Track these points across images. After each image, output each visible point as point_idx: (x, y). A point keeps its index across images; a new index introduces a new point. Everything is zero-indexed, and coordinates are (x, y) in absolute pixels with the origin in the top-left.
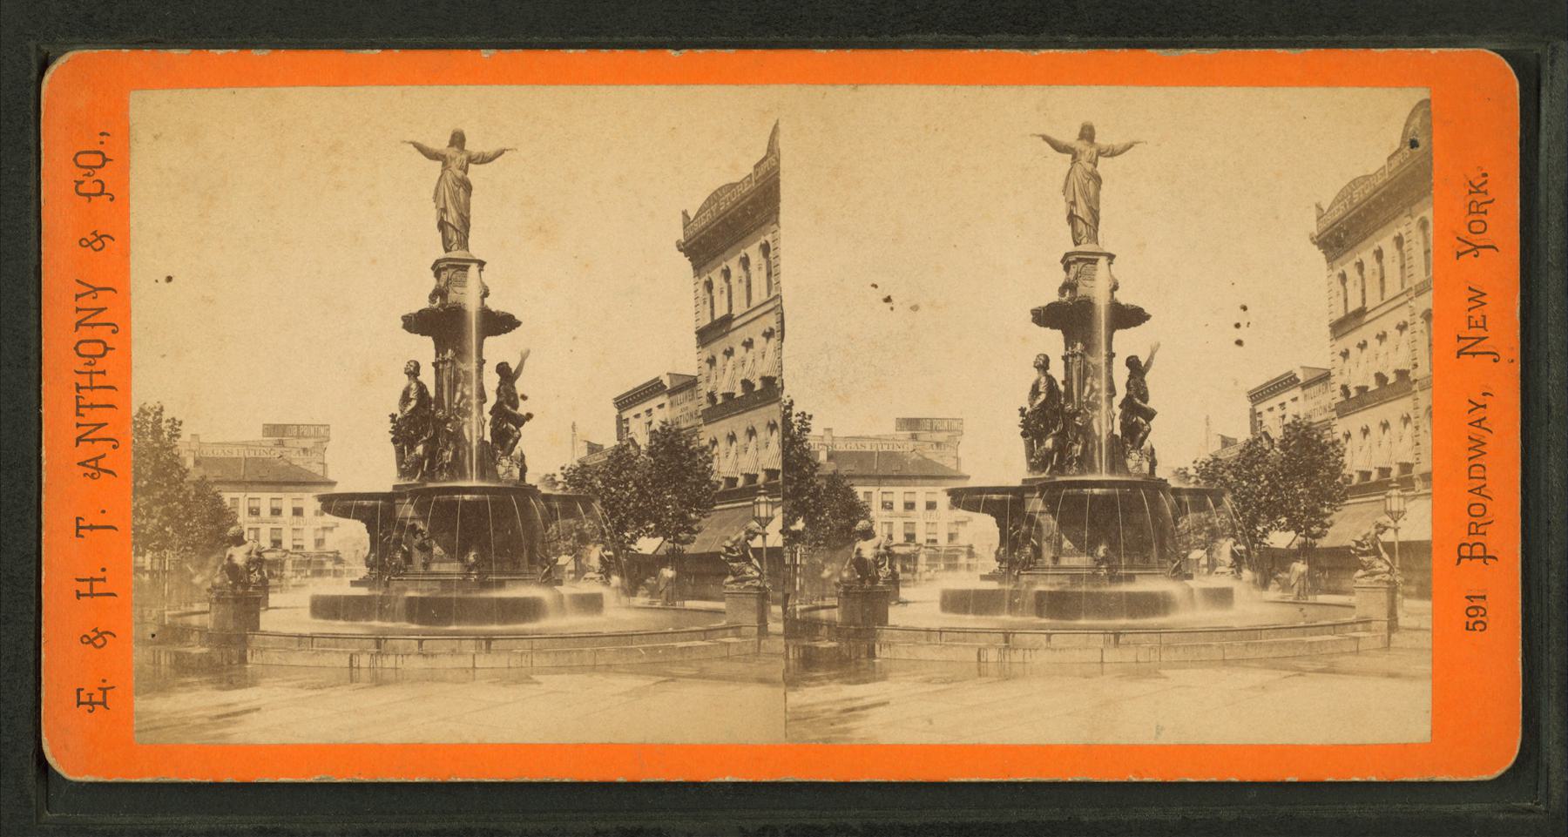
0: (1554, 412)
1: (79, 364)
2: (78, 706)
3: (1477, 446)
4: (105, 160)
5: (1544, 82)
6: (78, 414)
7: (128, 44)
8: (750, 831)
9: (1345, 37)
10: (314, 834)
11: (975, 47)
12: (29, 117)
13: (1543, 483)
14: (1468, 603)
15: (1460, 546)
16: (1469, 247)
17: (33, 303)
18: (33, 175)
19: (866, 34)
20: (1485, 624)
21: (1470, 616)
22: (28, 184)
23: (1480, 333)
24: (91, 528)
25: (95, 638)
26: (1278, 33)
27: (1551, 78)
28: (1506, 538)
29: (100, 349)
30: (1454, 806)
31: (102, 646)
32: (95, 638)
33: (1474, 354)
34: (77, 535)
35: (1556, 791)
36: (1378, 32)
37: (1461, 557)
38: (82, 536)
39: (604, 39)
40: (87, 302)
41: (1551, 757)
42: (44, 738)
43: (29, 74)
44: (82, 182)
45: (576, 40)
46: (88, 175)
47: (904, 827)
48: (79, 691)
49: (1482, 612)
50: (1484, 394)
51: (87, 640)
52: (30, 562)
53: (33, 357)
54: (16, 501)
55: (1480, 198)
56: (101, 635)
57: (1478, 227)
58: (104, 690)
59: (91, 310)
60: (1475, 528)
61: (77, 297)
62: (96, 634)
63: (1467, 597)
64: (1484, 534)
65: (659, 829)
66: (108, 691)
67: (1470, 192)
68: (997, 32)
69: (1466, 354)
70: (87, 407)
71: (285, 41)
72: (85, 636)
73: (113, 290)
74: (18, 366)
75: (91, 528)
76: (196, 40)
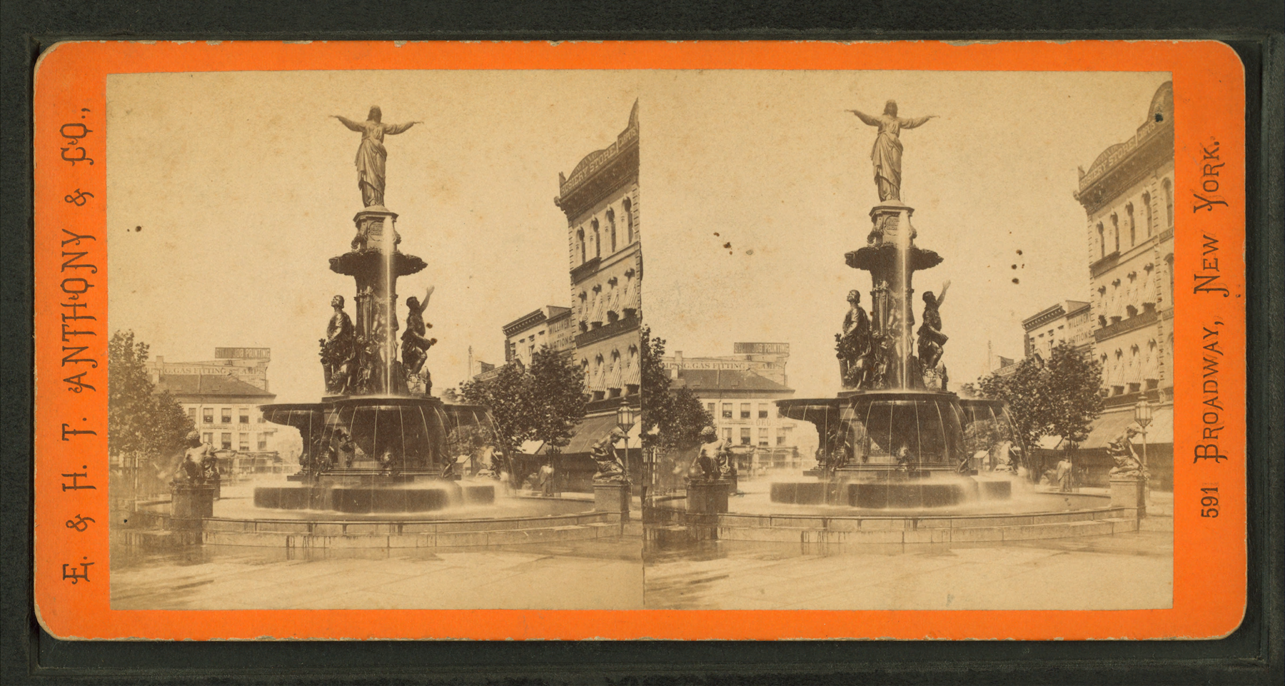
0: (1274, 338)
1: (65, 298)
2: (64, 579)
3: (1211, 365)
4: (86, 131)
6: (64, 339)
7: (105, 36)
8: (615, 681)
9: (1102, 30)
10: (258, 683)
11: (799, 39)
13: (1264, 396)
14: (1203, 494)
16: (1204, 203)
17: (27, 248)
18: (27, 144)
19: (710, 28)
20: (1217, 512)
22: (23, 151)
23: (1213, 273)
24: (75, 432)
25: (78, 523)
26: (1047, 27)
27: (1271, 64)
28: (1234, 441)
29: (80, 131)
31: (83, 204)
32: (78, 523)
33: (1208, 290)
34: (63, 439)
36: (1129, 26)
37: (1197, 457)
38: (67, 440)
39: (495, 32)
40: (71, 248)
42: (36, 605)
44: (67, 149)
46: (72, 143)
47: (741, 678)
48: (65, 566)
49: (1214, 502)
50: (1216, 323)
51: (71, 524)
52: (25, 460)
53: (27, 293)
55: (1213, 162)
56: (82, 520)
57: (1211, 186)
58: (85, 566)
59: (75, 254)
61: (63, 243)
62: (78, 520)
63: (1202, 490)
65: (540, 680)
66: (89, 567)
67: (1205, 158)
68: (817, 26)
69: (1201, 290)
71: (233, 33)
72: (70, 521)
74: (15, 300)
75: (75, 432)
76: (160, 33)
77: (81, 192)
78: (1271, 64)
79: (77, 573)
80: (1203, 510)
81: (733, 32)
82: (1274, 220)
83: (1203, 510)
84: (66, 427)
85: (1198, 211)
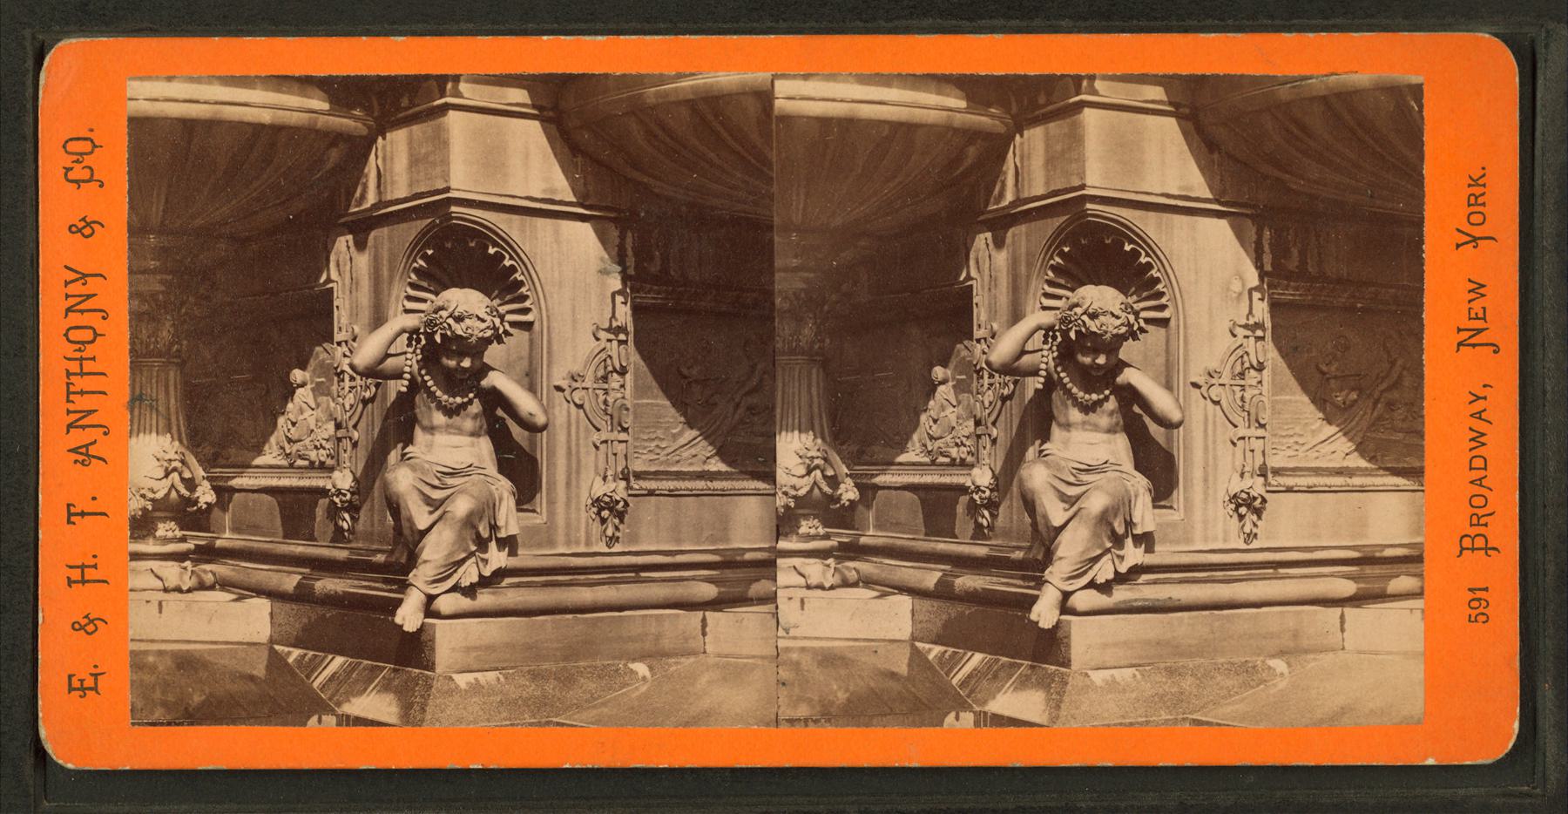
0: (1549, 396)
1: (70, 350)
3: (1478, 438)
4: (95, 146)
5: (1539, 65)
6: (68, 401)
7: (123, 33)
9: (1338, 21)
14: (1471, 595)
21: (1483, 614)
23: (1479, 324)
24: (83, 514)
26: (1272, 17)
28: (1505, 530)
30: (1452, 790)
33: (1474, 345)
34: (69, 522)
35: (1553, 776)
36: (1372, 16)
37: (1462, 549)
39: (599, 25)
43: (25, 62)
44: (72, 169)
46: (77, 161)
49: (1484, 603)
50: (1485, 386)
55: (1477, 190)
58: (96, 676)
59: (80, 296)
60: (1476, 520)
61: (67, 283)
62: (86, 621)
63: (1470, 590)
64: (1486, 525)
66: (99, 677)
68: (991, 18)
70: (77, 514)
71: (280, 28)
74: (15, 355)
75: (83, 514)
77: (88, 220)
79: (86, 684)
80: (1470, 616)
81: (890, 25)
82: (1550, 252)
83: (1470, 616)
84: (72, 508)
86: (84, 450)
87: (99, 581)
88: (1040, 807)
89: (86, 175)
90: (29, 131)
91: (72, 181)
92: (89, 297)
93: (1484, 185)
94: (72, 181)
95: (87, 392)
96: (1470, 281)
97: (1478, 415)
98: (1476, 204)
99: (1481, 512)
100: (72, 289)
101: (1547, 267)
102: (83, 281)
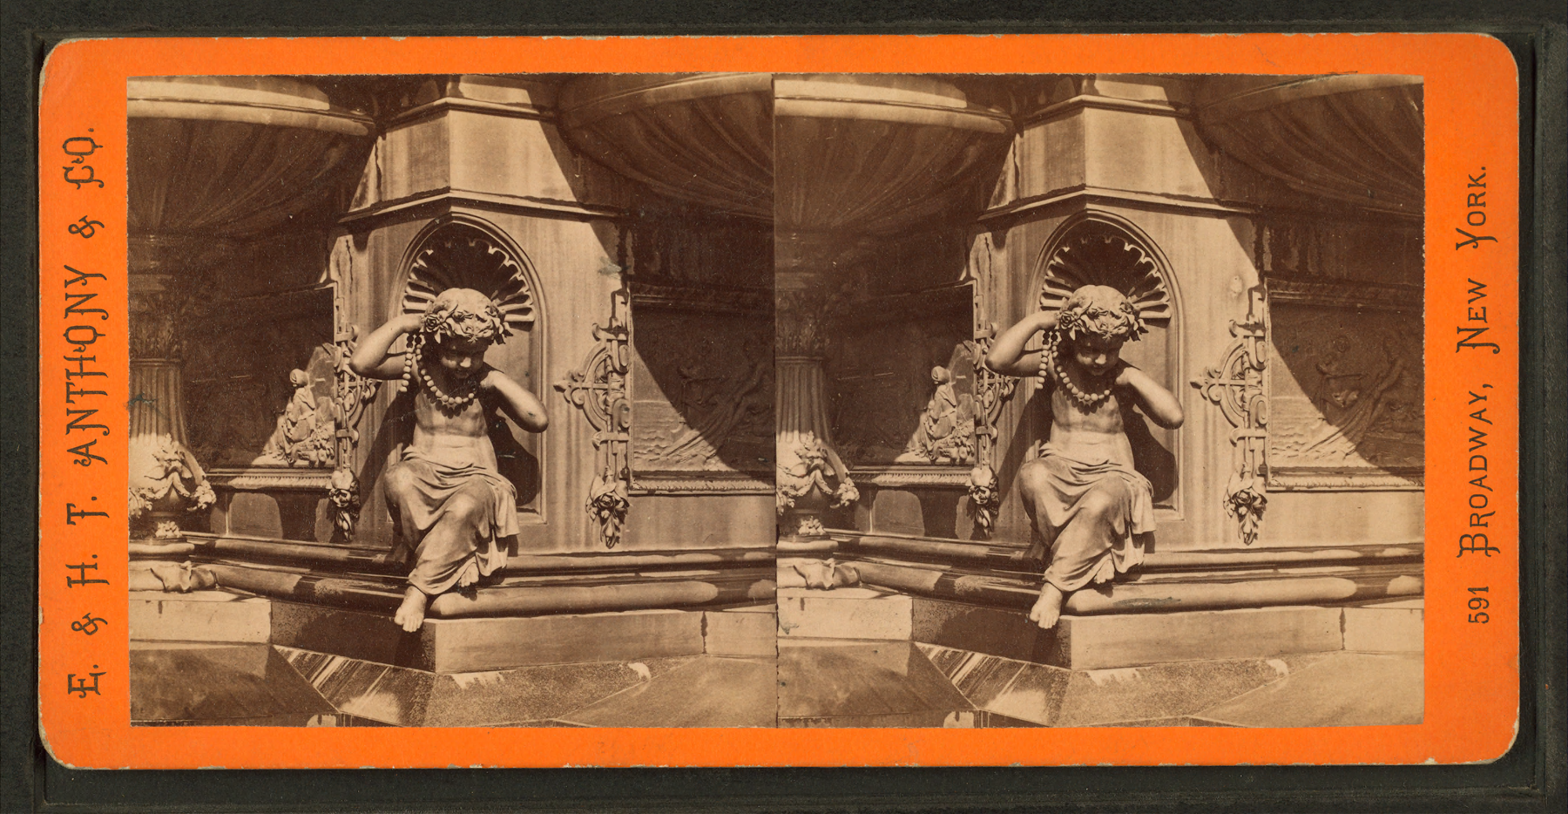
0: (1549, 396)
1: (70, 350)
2: (69, 692)
3: (1478, 438)
4: (95, 146)
5: (1539, 65)
6: (68, 401)
12: (25, 106)
14: (1471, 595)
15: (1462, 537)
16: (1468, 239)
19: (861, 20)
21: (1483, 614)
23: (1479, 324)
24: (83, 514)
26: (1272, 17)
28: (1505, 530)
30: (1452, 790)
32: (86, 625)
33: (1474, 345)
34: (69, 522)
36: (1372, 16)
37: (1462, 549)
38: (74, 523)
39: (599, 26)
40: (76, 288)
41: (1547, 741)
44: (72, 169)
45: (571, 27)
46: (77, 161)
49: (1484, 604)
50: (1485, 386)
52: (27, 551)
54: (13, 490)
55: (1477, 190)
58: (95, 676)
60: (1477, 520)
63: (1469, 590)
64: (1486, 525)
70: (77, 514)
71: (280, 28)
73: (101, 275)
75: (83, 514)
76: (190, 28)
77: (88, 220)
78: (1546, 61)
79: (86, 684)
81: (890, 25)
85: (1460, 248)
86: (83, 450)
87: (99, 581)
88: (1040, 807)
89: (86, 174)
90: (29, 131)
91: (72, 181)
92: (89, 297)
93: (1484, 185)
94: (72, 181)
95: (87, 392)
96: (1470, 280)
97: (1478, 415)
98: (1476, 204)
99: (1480, 512)
100: (72, 289)
101: (1547, 267)
102: (83, 281)
